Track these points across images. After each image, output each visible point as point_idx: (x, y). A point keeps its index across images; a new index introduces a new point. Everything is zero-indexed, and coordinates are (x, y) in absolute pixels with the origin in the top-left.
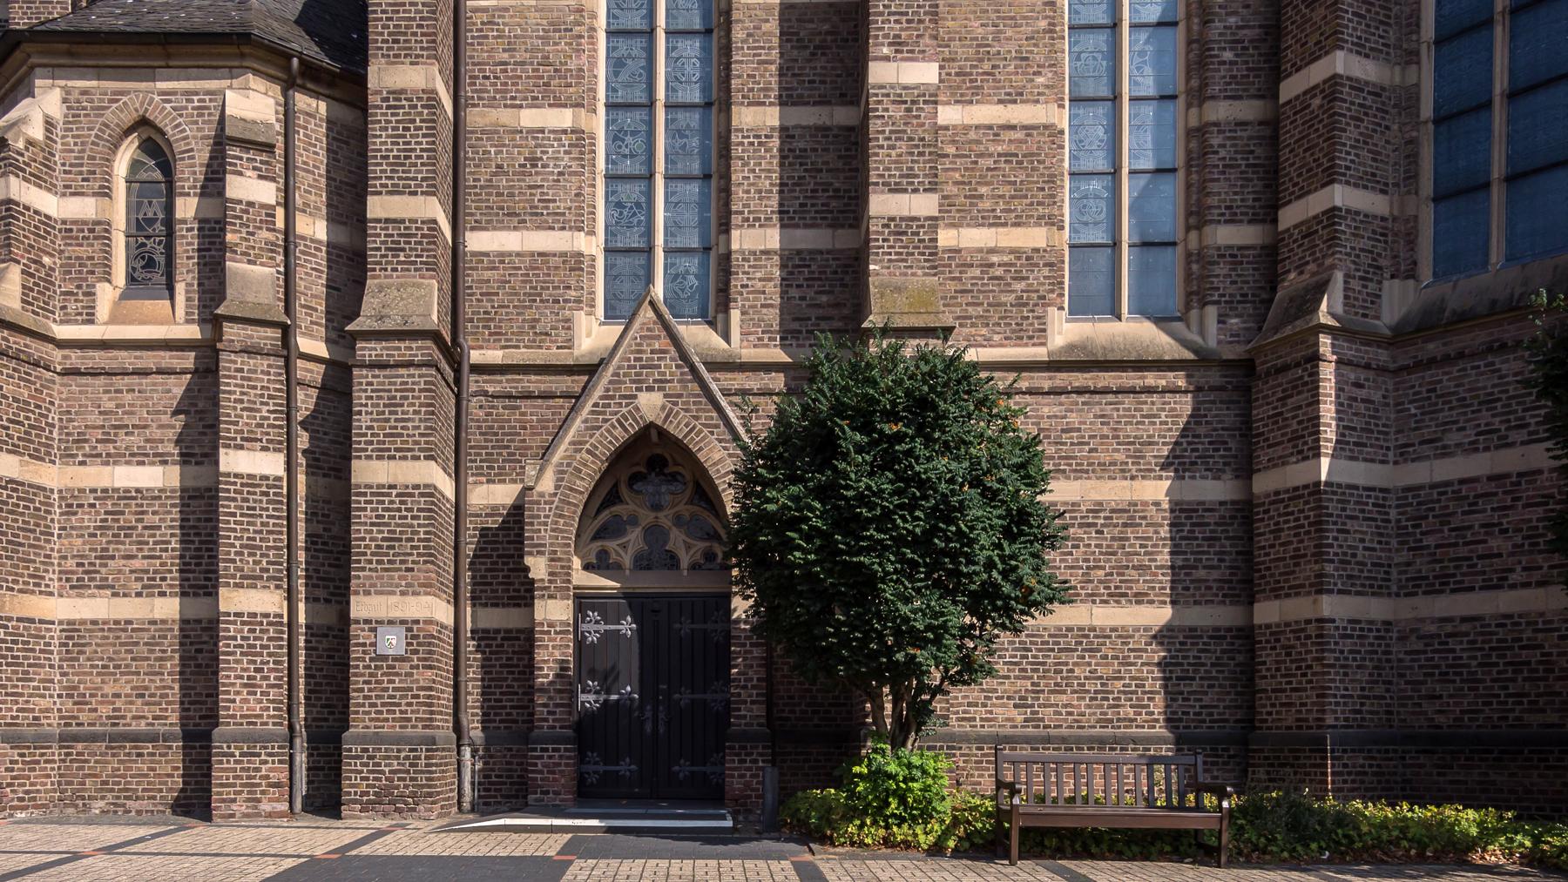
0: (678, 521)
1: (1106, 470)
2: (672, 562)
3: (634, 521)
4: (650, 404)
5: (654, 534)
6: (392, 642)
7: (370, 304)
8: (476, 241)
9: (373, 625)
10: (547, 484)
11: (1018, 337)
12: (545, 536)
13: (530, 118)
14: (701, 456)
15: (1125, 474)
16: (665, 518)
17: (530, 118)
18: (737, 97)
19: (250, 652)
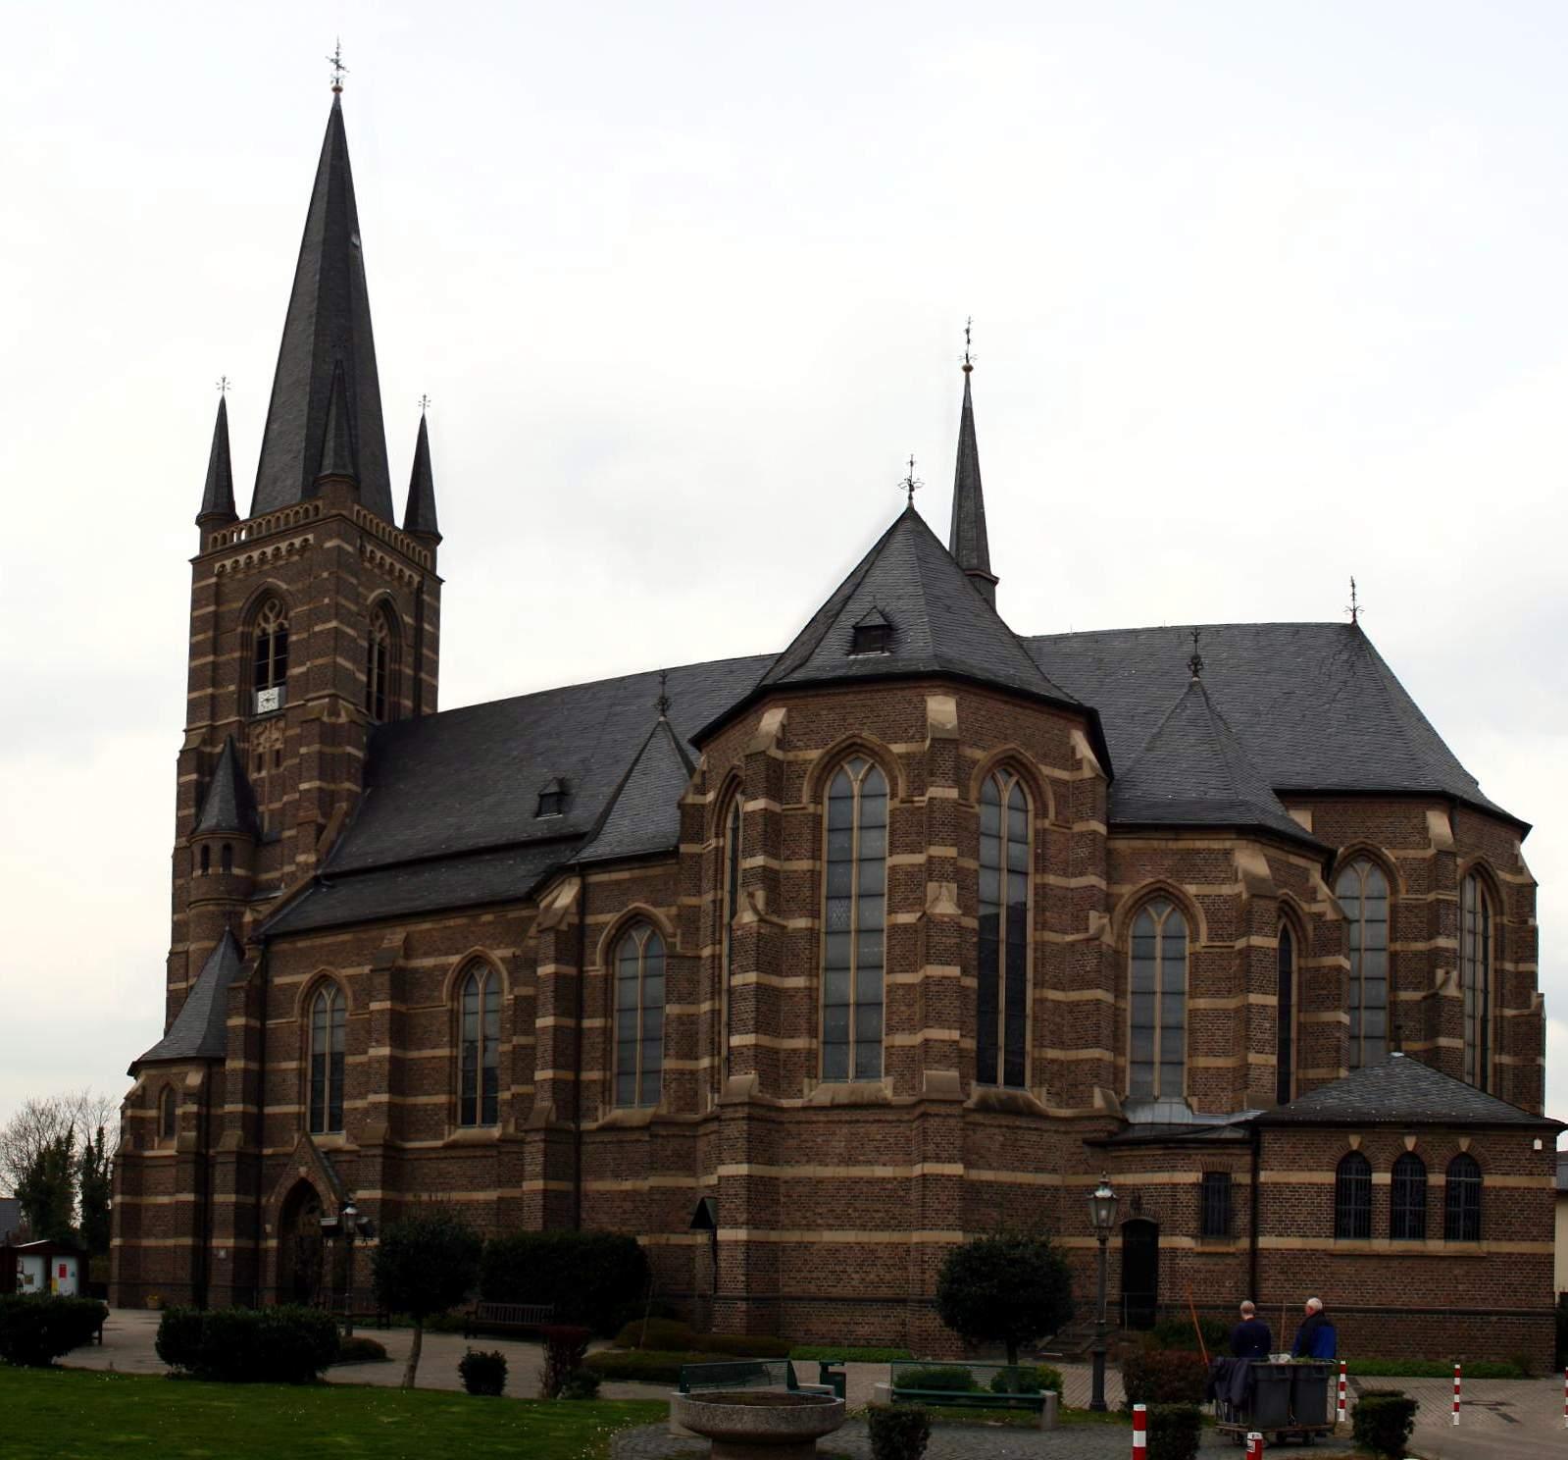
4: (303, 1170)
6: (222, 1254)
15: (467, 1189)
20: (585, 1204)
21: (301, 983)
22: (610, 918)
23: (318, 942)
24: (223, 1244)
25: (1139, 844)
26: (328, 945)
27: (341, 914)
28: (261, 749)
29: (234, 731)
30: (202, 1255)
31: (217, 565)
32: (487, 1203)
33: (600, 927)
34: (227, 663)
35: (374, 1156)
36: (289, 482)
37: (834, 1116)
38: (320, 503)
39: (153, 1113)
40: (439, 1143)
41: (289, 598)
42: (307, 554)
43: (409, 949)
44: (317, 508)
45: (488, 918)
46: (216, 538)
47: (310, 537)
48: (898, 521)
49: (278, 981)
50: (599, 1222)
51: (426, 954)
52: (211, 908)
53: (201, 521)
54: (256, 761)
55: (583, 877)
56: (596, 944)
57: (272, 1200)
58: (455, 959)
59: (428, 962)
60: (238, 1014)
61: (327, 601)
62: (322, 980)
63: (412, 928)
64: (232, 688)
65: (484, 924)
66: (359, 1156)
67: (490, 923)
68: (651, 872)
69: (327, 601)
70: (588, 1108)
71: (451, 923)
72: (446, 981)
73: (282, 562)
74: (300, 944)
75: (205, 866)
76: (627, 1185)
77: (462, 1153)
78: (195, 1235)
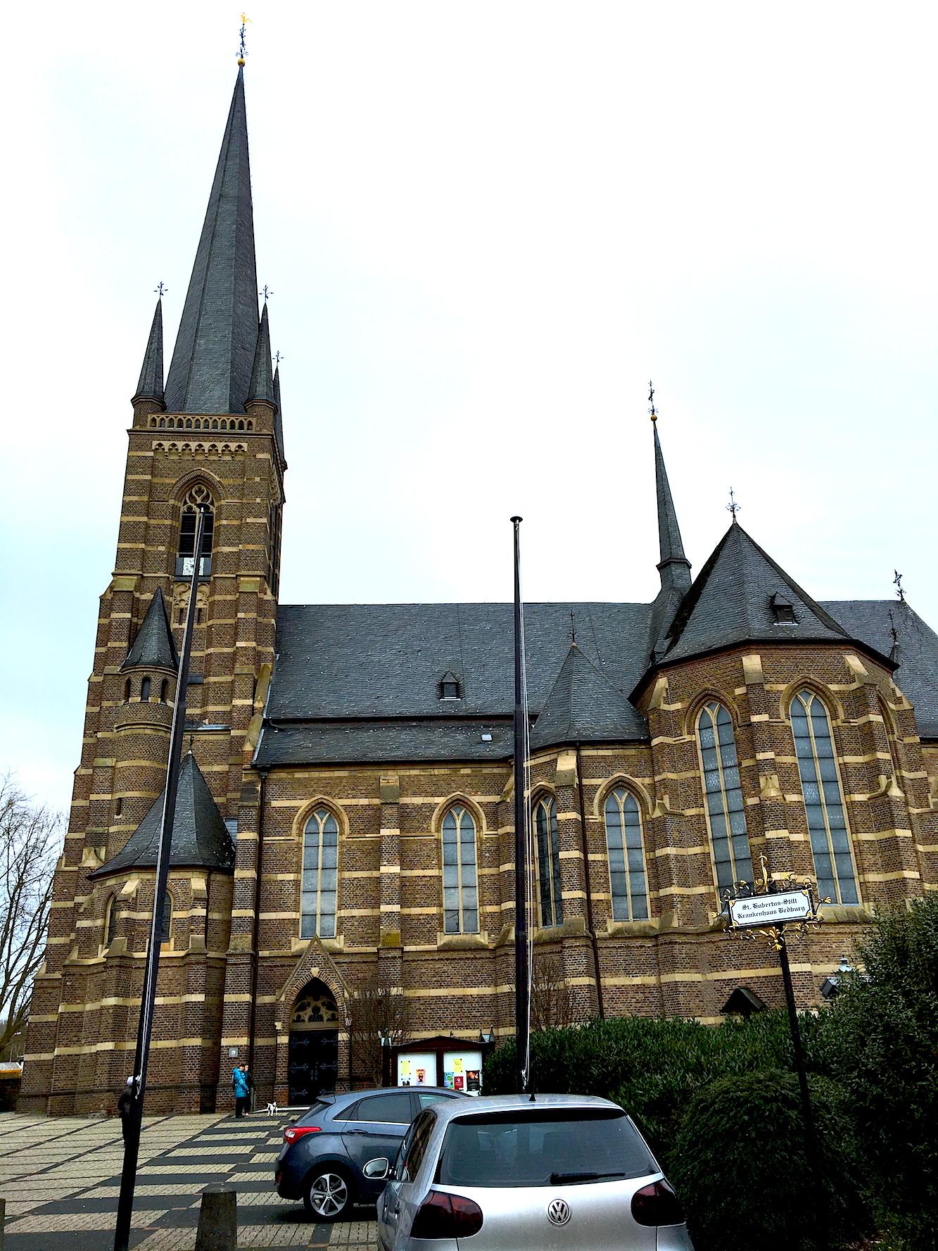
0: (323, 1004)
1: (455, 985)
2: (321, 1018)
3: (309, 1004)
4: (315, 971)
5: (316, 1010)
6: (234, 1053)
7: (232, 944)
8: (585, 782)
9: (228, 1047)
10: (283, 999)
11: (429, 942)
12: (282, 1016)
13: (280, 877)
14: (364, 1224)
15: (462, 986)
16: (319, 1004)
17: (280, 877)
18: (227, 989)
19: (192, 1058)
20: (606, 996)
21: (299, 808)
22: (602, 782)
23: (315, 774)
24: (234, 1042)
25: (306, 775)
26: (325, 779)
27: (347, 753)
28: (183, 605)
29: (162, 583)
30: (213, 1056)
31: (155, 443)
32: (481, 997)
33: (596, 787)
34: (159, 527)
35: (394, 958)
36: (217, 393)
37: (839, 929)
38: (254, 421)
39: (145, 915)
40: (434, 947)
41: (221, 490)
42: (238, 458)
43: (402, 790)
44: (250, 423)
45: (467, 771)
46: (154, 420)
47: (245, 445)
48: (277, 563)
49: (274, 804)
50: (618, 1010)
51: (414, 794)
52: (148, 732)
53: (135, 401)
54: (178, 614)
55: (578, 750)
56: (592, 800)
57: (283, 999)
58: (440, 800)
59: (418, 800)
60: (249, 829)
61: (258, 500)
62: (320, 806)
63: (402, 773)
64: (162, 548)
65: (463, 776)
66: (380, 958)
67: (468, 775)
68: (628, 752)
69: (258, 500)
70: (598, 922)
71: (436, 772)
72: (434, 818)
73: (216, 458)
74: (297, 775)
75: (127, 696)
76: (637, 981)
77: (455, 955)
78: (203, 1034)
